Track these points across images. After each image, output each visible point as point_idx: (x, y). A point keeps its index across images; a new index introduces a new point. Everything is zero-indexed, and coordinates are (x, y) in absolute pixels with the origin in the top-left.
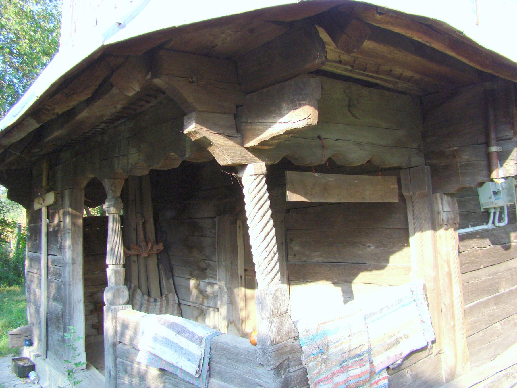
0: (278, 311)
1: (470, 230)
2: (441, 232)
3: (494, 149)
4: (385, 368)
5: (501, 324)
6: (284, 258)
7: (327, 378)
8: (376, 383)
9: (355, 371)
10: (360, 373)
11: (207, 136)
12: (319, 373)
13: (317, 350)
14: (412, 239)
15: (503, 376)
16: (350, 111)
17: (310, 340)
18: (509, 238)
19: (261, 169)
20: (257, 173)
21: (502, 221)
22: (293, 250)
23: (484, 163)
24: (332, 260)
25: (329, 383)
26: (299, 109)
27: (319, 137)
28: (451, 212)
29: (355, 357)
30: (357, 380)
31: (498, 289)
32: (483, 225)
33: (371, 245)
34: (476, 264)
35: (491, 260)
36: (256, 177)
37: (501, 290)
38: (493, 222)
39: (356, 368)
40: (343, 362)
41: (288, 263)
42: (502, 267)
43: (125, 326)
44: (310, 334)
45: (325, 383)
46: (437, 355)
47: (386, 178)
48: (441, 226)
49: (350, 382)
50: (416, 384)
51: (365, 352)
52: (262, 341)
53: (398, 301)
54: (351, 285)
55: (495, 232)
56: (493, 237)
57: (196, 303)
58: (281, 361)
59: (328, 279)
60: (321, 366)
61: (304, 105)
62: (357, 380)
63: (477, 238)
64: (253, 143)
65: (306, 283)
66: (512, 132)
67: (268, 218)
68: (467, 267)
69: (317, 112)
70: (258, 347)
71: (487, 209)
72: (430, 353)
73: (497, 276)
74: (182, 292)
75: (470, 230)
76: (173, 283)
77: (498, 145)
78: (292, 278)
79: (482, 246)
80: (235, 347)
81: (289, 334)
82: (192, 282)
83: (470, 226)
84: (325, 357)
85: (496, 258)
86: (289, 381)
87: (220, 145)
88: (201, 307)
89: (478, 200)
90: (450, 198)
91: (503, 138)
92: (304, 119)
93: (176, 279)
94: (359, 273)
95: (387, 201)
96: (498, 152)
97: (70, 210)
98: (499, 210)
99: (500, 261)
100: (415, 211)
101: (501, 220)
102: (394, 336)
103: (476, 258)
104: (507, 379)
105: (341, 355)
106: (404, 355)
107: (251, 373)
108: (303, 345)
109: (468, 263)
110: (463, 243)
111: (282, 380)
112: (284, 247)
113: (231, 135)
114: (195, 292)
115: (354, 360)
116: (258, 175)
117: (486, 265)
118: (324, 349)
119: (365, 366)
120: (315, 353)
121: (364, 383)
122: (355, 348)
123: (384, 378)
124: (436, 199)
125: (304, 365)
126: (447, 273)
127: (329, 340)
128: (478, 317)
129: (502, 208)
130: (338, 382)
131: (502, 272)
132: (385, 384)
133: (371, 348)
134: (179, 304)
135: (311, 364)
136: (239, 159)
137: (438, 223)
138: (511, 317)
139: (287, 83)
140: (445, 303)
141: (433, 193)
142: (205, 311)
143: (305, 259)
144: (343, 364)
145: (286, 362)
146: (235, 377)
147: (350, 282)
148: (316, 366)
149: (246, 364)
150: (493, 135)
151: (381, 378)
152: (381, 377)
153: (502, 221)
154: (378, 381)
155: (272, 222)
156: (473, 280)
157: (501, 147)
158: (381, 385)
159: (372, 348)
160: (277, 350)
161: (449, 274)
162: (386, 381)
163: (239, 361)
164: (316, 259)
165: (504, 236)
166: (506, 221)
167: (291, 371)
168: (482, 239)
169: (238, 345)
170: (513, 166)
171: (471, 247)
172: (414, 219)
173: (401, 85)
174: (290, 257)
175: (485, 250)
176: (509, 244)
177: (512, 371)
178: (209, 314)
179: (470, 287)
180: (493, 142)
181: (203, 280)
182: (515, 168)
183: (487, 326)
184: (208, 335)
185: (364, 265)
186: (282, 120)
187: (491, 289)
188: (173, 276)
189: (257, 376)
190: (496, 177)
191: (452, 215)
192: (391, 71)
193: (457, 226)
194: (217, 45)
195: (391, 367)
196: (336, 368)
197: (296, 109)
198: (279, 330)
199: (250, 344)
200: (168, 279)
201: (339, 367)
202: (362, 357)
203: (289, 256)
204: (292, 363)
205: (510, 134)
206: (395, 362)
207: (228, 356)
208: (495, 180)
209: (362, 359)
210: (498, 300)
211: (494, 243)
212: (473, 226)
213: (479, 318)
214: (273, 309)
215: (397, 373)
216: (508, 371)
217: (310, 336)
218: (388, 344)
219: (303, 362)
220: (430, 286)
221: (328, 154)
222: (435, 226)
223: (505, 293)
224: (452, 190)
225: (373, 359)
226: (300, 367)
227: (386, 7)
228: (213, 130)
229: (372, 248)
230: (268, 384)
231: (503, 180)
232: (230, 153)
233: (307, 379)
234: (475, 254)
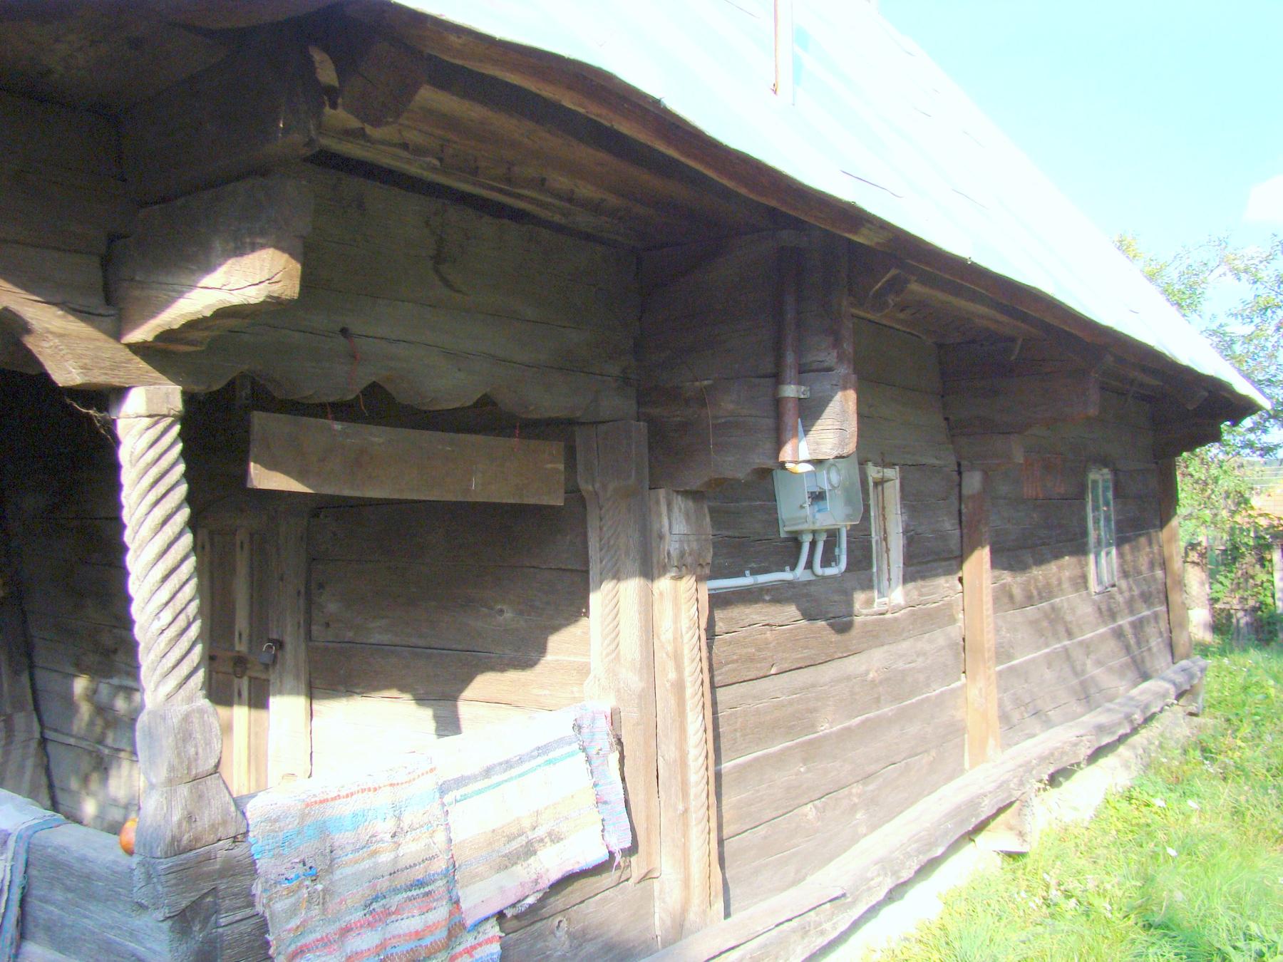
0: (189, 769)
1: (747, 581)
2: (664, 584)
4: (493, 916)
5: (815, 807)
6: (302, 631)
7: (326, 940)
8: (469, 951)
9: (411, 923)
10: (420, 927)
11: (14, 306)
12: (301, 930)
13: (300, 869)
15: (794, 932)
16: (437, 271)
17: (280, 844)
18: (850, 603)
19: (168, 402)
20: (155, 413)
21: (833, 564)
22: (323, 612)
23: (770, 422)
24: (413, 641)
25: (330, 953)
26: (251, 256)
27: (344, 331)
28: (691, 538)
29: (410, 887)
30: (413, 946)
31: (813, 726)
32: (784, 571)
33: (505, 607)
34: (759, 665)
35: (800, 656)
36: (148, 421)
37: (822, 728)
38: (809, 565)
39: (410, 914)
40: (376, 899)
41: (311, 644)
42: (827, 673)
44: (279, 827)
45: (318, 954)
46: (643, 884)
47: (533, 444)
48: (664, 570)
49: (394, 951)
50: (583, 953)
51: (438, 874)
52: (144, 845)
53: (538, 748)
54: (456, 706)
55: (812, 589)
56: (808, 601)
57: (86, 740)
58: (194, 896)
59: (403, 689)
60: (308, 909)
61: (263, 247)
62: (412, 945)
63: (764, 601)
64: (143, 333)
65: (351, 696)
66: (835, 354)
67: (177, 529)
68: (734, 670)
69: (299, 266)
70: (136, 859)
71: (796, 532)
72: (623, 878)
73: (814, 694)
74: (52, 709)
75: (747, 581)
76: (28, 684)
77: (799, 383)
78: (318, 681)
79: (778, 620)
80: (83, 859)
81: (220, 829)
82: (80, 685)
83: (747, 572)
84: (320, 887)
85: (813, 652)
86: (215, 947)
87: (52, 333)
88: (99, 750)
89: (775, 510)
90: (691, 504)
91: (814, 366)
92: (260, 283)
93: (39, 674)
95: (532, 501)
96: (800, 399)
98: (823, 537)
99: (824, 658)
100: (605, 529)
101: (828, 560)
102: (519, 835)
103: (759, 650)
104: (803, 938)
105: (370, 882)
106: (545, 883)
107: (120, 928)
108: (259, 856)
109: (737, 661)
110: (725, 612)
111: (193, 945)
112: (302, 602)
113: (86, 309)
114: (85, 709)
115: (405, 895)
116: (156, 418)
117: (786, 666)
118: (320, 866)
119: (434, 911)
120: (293, 876)
121: (433, 951)
122: (410, 866)
123: (489, 941)
124: (658, 502)
125: (259, 908)
126: (672, 685)
127: (337, 844)
128: (758, 791)
129: (833, 536)
130: (359, 950)
131: (826, 685)
132: (492, 954)
133: (454, 866)
134: (43, 741)
135: (280, 906)
136: (106, 374)
137: (658, 562)
138: (846, 791)
139: (230, 187)
140: (667, 757)
141: (650, 489)
142: (106, 759)
143: (350, 634)
144: (375, 905)
145: (209, 899)
146: (83, 937)
147: (455, 698)
148: (294, 911)
149: (109, 903)
150: (790, 358)
151: (481, 940)
152: (481, 938)
153: (833, 564)
154: (474, 948)
155: (188, 539)
156: (750, 701)
157: (808, 388)
158: (482, 957)
159: (457, 866)
160: (182, 867)
161: (679, 686)
162: (495, 948)
163: (91, 896)
164: (377, 638)
165: (836, 598)
167: (223, 921)
168: (778, 605)
169: (91, 854)
170: (831, 436)
171: (746, 622)
172: (601, 550)
173: (584, 220)
174: (315, 629)
175: (784, 630)
176: (849, 618)
177: (817, 919)
178: (119, 766)
179: (740, 720)
180: (790, 372)
181: (107, 681)
182: (836, 441)
183: (780, 812)
184: (24, 826)
185: (489, 657)
186: (208, 280)
187: (794, 725)
188: (32, 667)
189: (133, 934)
190: (790, 459)
191: (695, 543)
192: (544, 180)
193: (707, 571)
194: (50, 71)
195: (509, 913)
196: (354, 915)
197: (242, 255)
198: (190, 818)
199: (121, 852)
200: (16, 673)
201: (363, 912)
202: (427, 889)
203: (314, 628)
204: (227, 902)
205: (830, 358)
206: (519, 901)
207: (68, 883)
208: (788, 466)
209: (428, 894)
210: (811, 751)
211: (809, 616)
212: (755, 572)
213: (761, 794)
214: (176, 762)
215: (528, 928)
216: (808, 919)
217: (281, 834)
218: (504, 857)
219: (257, 900)
220: (631, 715)
221: (364, 376)
222: (649, 570)
223: (831, 733)
224: (696, 483)
225: (460, 894)
226: (248, 912)
227: (444, 18)
228: (33, 293)
229: (509, 615)
230: (158, 957)
231: (809, 467)
232: (80, 357)
233: (267, 944)
234: (756, 639)
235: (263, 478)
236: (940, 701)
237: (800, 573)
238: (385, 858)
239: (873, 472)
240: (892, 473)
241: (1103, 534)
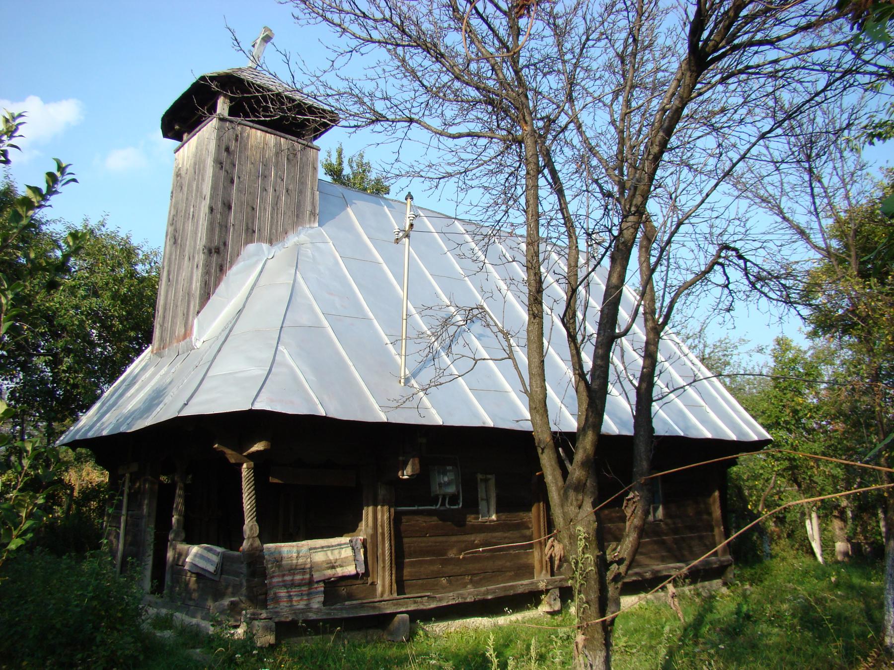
12: (274, 572)
38: (443, 504)
43: (180, 555)
97: (150, 477)
135: (269, 566)
148: (272, 567)
161: (383, 534)
162: (323, 589)
166: (460, 506)
212: (419, 506)
220: (369, 541)
235: (272, 480)
238: (295, 562)
241: (193, 201)
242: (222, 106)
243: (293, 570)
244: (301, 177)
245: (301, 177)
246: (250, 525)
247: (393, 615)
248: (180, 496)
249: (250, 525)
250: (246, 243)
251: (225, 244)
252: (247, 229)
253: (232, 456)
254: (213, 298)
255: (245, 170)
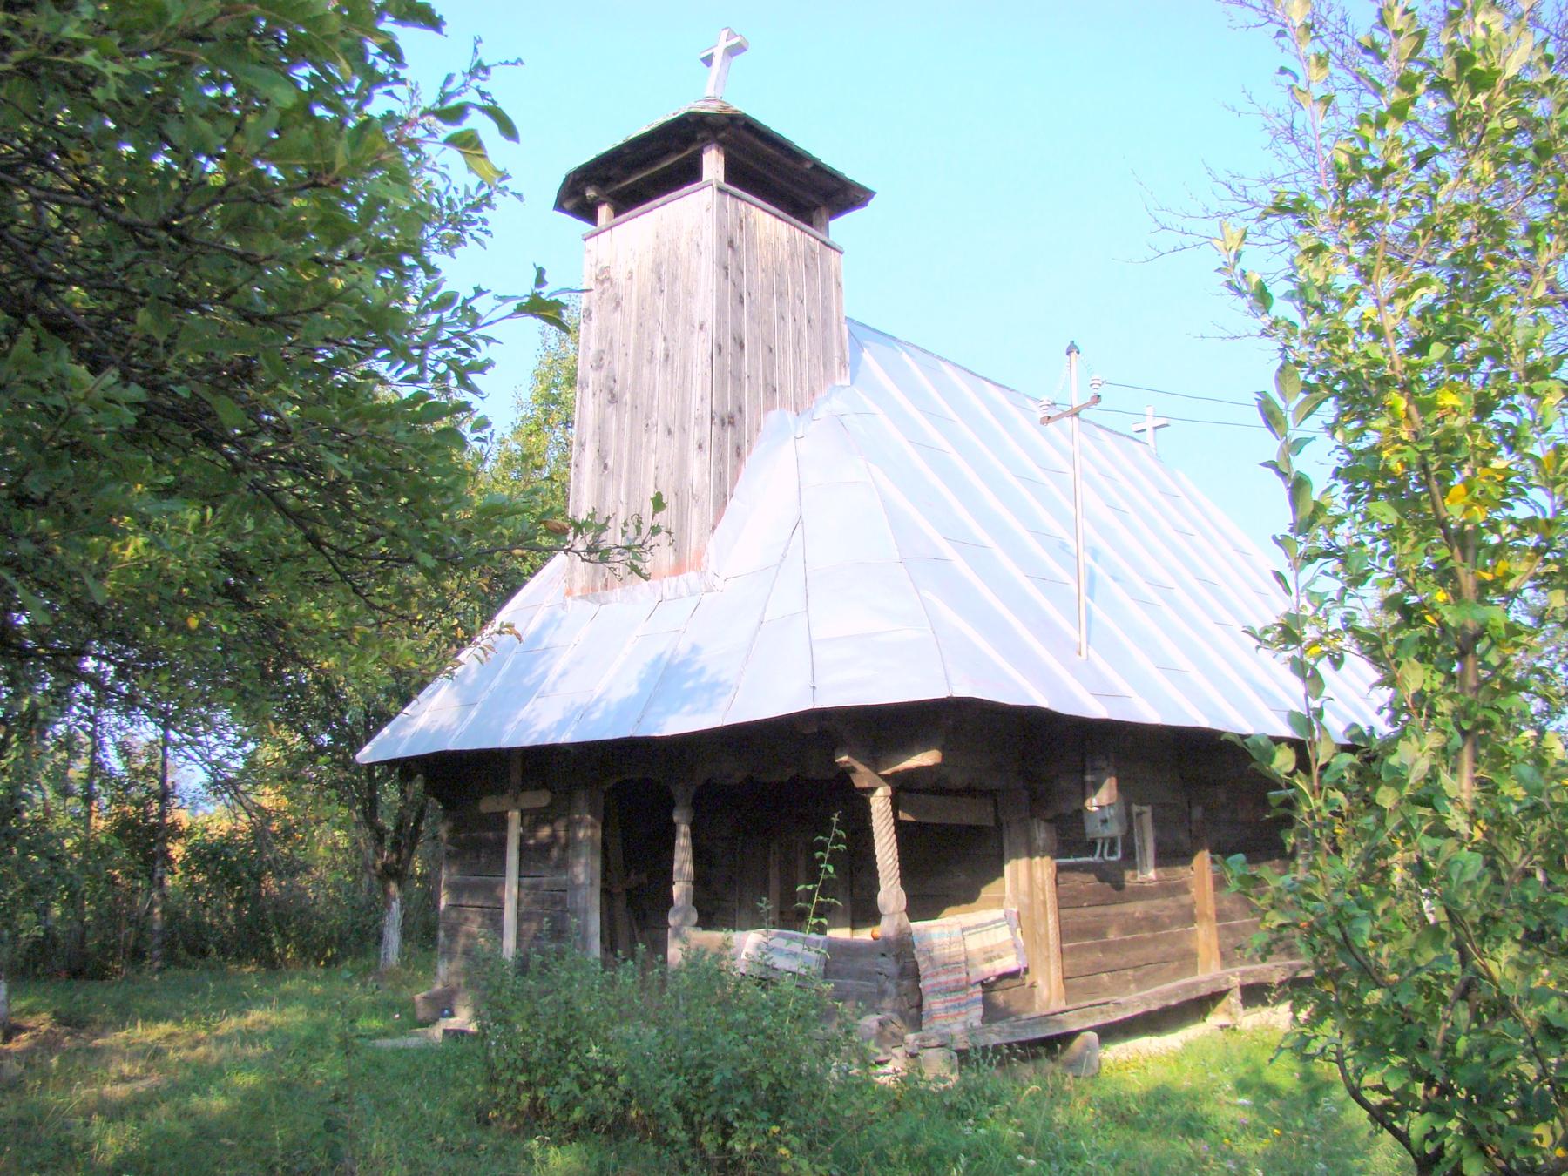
1: (1071, 860)
2: (1037, 859)
3: (1088, 778)
14: (1007, 868)
38: (1101, 855)
42: (1113, 909)
48: (1037, 854)
75: (1071, 860)
94: (948, 910)
101: (1112, 852)
150: (1088, 765)
161: (1044, 903)
166: (1119, 855)
205: (1104, 764)
211: (1102, 880)
222: (1031, 854)
236: (1180, 937)
237: (1096, 858)
239: (1135, 809)
240: (1147, 809)
242: (713, 163)
243: (949, 966)
244: (824, 299)
245: (824, 299)
246: (891, 893)
247: (1075, 1034)
248: (684, 849)
249: (891, 893)
250: (767, 410)
251: (740, 410)
252: (766, 385)
253: (863, 777)
254: (733, 504)
255: (755, 281)
